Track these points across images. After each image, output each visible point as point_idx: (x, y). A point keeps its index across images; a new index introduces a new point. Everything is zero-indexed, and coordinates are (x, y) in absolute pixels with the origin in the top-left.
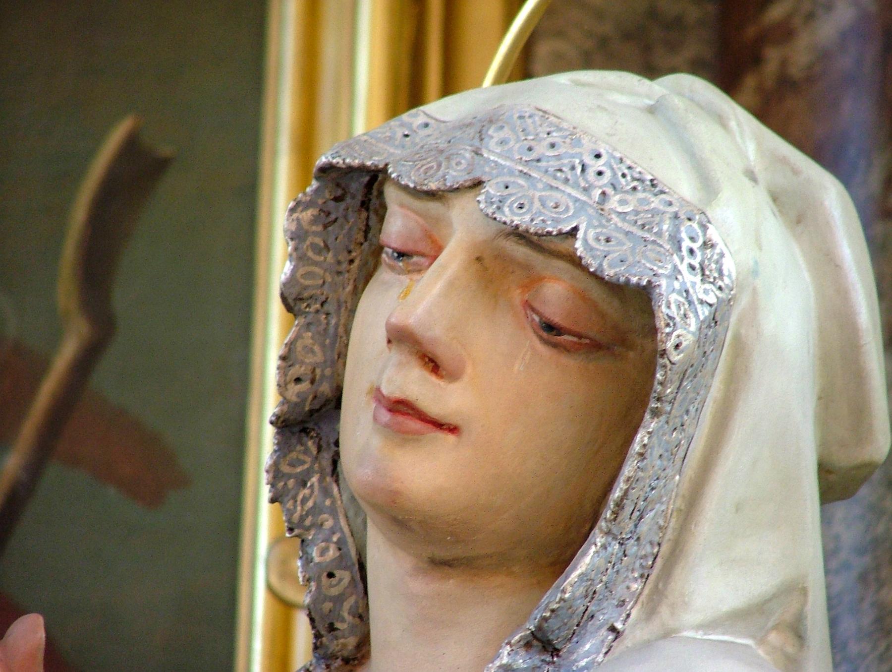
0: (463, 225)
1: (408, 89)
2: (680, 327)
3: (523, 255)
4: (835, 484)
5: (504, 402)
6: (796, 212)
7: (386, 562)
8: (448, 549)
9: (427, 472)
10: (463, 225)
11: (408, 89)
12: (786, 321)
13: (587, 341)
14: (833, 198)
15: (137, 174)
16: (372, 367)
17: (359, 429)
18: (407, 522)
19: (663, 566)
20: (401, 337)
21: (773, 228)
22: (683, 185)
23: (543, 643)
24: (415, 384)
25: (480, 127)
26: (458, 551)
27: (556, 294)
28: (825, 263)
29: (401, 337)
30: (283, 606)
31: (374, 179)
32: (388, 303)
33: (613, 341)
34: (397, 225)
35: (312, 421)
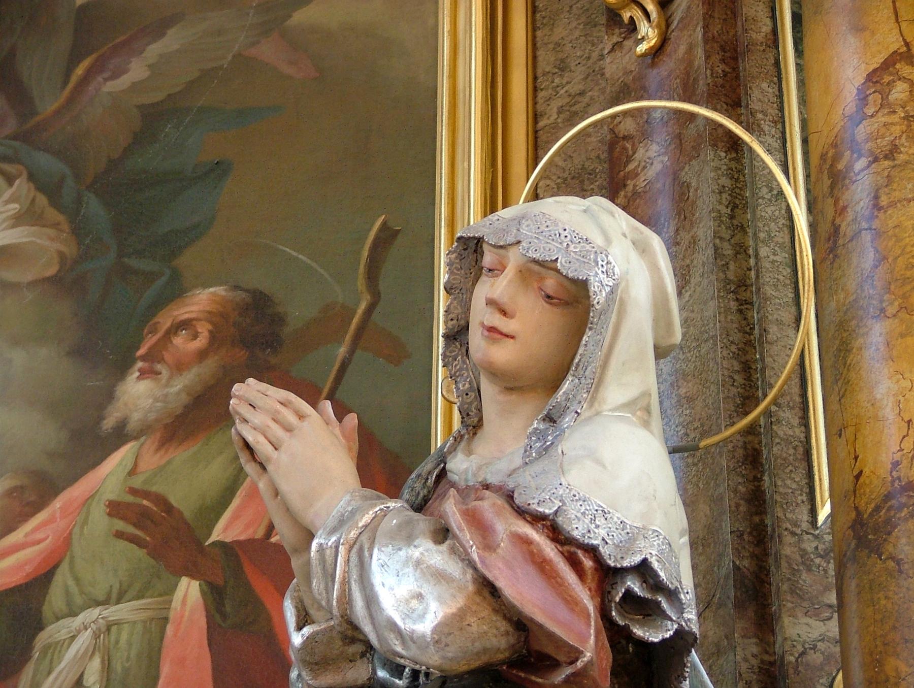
0: (514, 258)
1: (490, 207)
2: (599, 296)
3: (537, 270)
4: (660, 353)
5: (523, 330)
6: (642, 248)
7: (488, 389)
8: (512, 383)
9: (503, 354)
10: (514, 258)
11: (490, 207)
14: (656, 243)
15: (387, 237)
16: (480, 315)
17: (476, 338)
18: (496, 374)
19: (595, 387)
20: (491, 302)
21: (634, 255)
22: (599, 241)
23: (550, 419)
25: (519, 220)
27: (551, 284)
28: (654, 268)
29: (491, 302)
31: (479, 241)
32: (485, 289)
33: (574, 302)
34: (488, 259)
35: (458, 335)
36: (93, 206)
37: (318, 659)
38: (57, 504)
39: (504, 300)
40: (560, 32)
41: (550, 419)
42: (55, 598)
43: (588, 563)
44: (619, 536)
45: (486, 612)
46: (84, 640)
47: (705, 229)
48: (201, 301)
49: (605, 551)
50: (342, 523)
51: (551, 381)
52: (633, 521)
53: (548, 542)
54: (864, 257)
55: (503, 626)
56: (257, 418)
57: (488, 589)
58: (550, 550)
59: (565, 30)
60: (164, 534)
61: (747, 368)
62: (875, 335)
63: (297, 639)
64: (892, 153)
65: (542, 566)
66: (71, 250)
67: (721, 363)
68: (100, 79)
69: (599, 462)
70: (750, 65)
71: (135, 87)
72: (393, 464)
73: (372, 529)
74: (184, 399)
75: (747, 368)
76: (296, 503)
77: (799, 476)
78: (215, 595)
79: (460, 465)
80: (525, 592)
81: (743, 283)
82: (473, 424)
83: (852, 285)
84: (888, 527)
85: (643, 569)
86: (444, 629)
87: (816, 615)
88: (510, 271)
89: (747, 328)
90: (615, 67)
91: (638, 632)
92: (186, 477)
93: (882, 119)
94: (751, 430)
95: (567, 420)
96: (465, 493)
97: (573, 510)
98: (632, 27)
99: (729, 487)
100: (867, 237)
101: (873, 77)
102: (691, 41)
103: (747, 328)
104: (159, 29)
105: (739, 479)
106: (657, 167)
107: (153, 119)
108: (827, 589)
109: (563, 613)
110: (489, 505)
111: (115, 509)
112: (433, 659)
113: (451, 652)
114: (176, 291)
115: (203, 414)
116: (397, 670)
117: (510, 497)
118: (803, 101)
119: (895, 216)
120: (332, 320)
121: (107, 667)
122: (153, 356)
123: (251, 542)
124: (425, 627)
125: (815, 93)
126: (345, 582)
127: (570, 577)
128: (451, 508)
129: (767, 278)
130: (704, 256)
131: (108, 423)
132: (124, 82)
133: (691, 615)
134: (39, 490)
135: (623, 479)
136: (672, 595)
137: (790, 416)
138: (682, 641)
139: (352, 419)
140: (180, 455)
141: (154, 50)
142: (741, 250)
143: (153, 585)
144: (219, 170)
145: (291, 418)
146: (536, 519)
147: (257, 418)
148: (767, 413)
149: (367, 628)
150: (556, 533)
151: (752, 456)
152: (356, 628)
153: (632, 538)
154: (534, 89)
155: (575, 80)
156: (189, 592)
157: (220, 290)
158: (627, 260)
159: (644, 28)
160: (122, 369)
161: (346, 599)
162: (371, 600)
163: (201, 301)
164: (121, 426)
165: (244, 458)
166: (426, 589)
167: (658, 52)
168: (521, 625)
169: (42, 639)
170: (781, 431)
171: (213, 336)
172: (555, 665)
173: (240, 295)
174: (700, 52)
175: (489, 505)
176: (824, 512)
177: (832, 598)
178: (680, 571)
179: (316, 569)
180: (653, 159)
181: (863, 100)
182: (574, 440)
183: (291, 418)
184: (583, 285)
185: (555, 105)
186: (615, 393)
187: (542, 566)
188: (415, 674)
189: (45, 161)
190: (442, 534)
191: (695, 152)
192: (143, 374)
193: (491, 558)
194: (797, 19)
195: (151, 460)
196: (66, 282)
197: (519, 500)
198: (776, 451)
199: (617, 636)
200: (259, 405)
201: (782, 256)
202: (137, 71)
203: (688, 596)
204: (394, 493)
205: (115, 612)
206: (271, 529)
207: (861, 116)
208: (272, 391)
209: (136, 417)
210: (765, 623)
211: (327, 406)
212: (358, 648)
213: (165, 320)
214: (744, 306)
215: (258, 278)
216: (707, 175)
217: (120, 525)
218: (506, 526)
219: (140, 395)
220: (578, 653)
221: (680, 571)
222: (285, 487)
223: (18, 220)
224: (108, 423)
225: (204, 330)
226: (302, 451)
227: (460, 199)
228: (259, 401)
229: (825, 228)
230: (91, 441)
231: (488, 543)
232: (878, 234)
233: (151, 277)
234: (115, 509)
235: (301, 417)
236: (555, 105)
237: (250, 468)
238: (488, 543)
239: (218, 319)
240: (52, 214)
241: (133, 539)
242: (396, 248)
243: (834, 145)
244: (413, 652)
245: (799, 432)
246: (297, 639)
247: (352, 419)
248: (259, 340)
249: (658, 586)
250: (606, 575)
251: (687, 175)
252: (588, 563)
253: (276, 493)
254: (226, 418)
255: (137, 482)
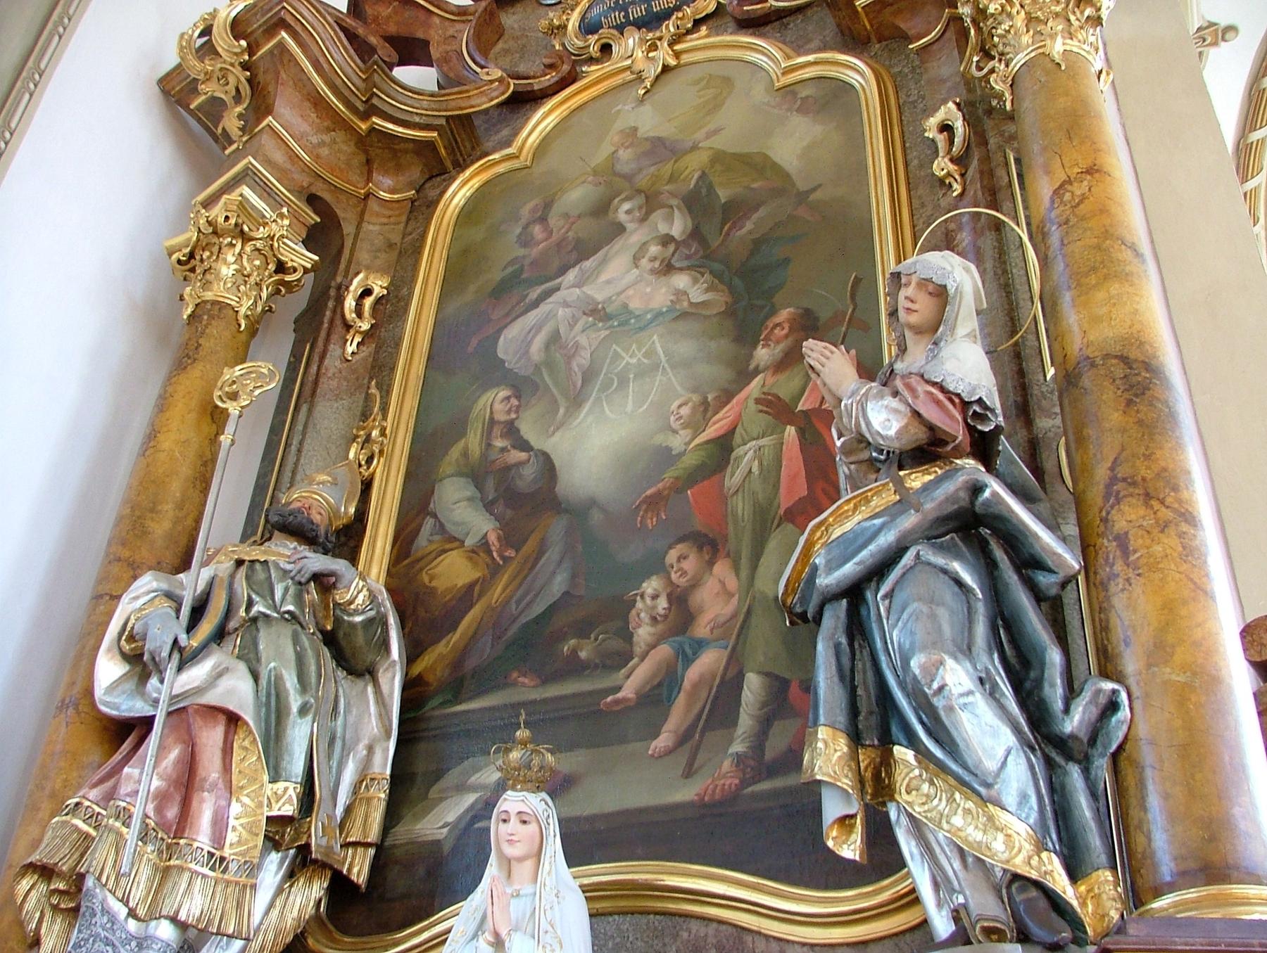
0: (914, 279)
1: (899, 262)
2: (951, 291)
3: (924, 283)
4: (978, 313)
5: (924, 307)
6: (967, 270)
7: (908, 334)
8: (918, 330)
9: (913, 319)
10: (914, 279)
11: (899, 262)
12: (968, 289)
13: (644, 507)
14: (973, 267)
15: (857, 281)
16: (902, 303)
17: (901, 313)
18: (911, 327)
19: (953, 329)
20: (906, 298)
21: (964, 273)
22: (949, 268)
23: (935, 343)
24: (910, 305)
25: (915, 263)
26: (532, 560)
27: (931, 288)
28: (973, 278)
29: (906, 298)
30: (890, 346)
31: (899, 273)
32: (903, 293)
33: (941, 294)
34: (903, 280)
35: (893, 314)
36: (737, 281)
37: (847, 451)
38: (734, 401)
39: (912, 297)
40: (920, 192)
41: (935, 343)
42: (737, 438)
43: (957, 401)
44: (968, 388)
45: (916, 424)
46: (751, 453)
47: (989, 265)
48: (784, 314)
49: (963, 395)
50: (853, 394)
51: (934, 329)
52: (974, 382)
53: (1116, 174)
54: (1059, 266)
55: (924, 429)
56: (814, 355)
57: (916, 414)
58: (941, 396)
59: (922, 191)
60: (779, 410)
61: (1012, 319)
62: (1067, 298)
63: (838, 443)
64: (1067, 222)
65: (938, 402)
66: (729, 300)
67: (1001, 318)
68: (491, 776)
69: (958, 359)
70: (1000, 196)
71: (750, 232)
72: (869, 369)
73: (866, 394)
74: (781, 355)
75: (1012, 319)
76: (833, 388)
77: (1038, 361)
78: (801, 432)
79: (899, 366)
80: (931, 414)
81: (1007, 285)
82: (903, 349)
83: (1055, 278)
84: (1079, 376)
85: (980, 401)
86: (899, 432)
87: (1050, 417)
88: (913, 284)
89: (1010, 303)
90: (944, 203)
91: (979, 427)
92: (785, 386)
93: (1062, 208)
94: (1016, 344)
95: (942, 344)
96: (903, 377)
97: (949, 380)
98: (950, 185)
99: (1010, 368)
100: (1060, 257)
101: (1056, 192)
102: (976, 188)
103: (1010, 303)
104: (756, 209)
105: (1014, 365)
106: (967, 241)
107: (758, 244)
108: (1054, 406)
109: (948, 421)
110: (914, 381)
111: (757, 401)
112: (896, 445)
113: (904, 441)
114: (773, 312)
115: (792, 358)
116: (881, 452)
117: (922, 376)
118: (1026, 208)
119: (1070, 248)
120: (837, 318)
121: (761, 464)
122: (767, 339)
123: (813, 410)
124: (892, 432)
125: (1032, 203)
126: (857, 418)
127: (950, 407)
128: (898, 383)
129: (1017, 281)
130: (990, 274)
131: (752, 367)
132: (744, 230)
133: (1001, 419)
134: (727, 396)
135: (968, 366)
136: (993, 411)
137: (1031, 337)
138: (998, 430)
139: (853, 352)
140: (782, 377)
141: (755, 216)
142: (1005, 272)
143: (777, 429)
144: (787, 261)
145: (828, 353)
146: (934, 384)
147: (814, 355)
148: (1022, 337)
149: (868, 436)
150: (942, 389)
151: (1017, 354)
152: (863, 436)
153: (973, 390)
154: (912, 215)
155: (929, 210)
156: (791, 431)
157: (792, 310)
158: (961, 275)
159: (955, 186)
160: (754, 346)
161: (858, 424)
162: (868, 424)
163: (784, 314)
164: (757, 366)
165: (810, 372)
166: (891, 417)
167: (962, 195)
168: (931, 428)
169: (734, 455)
170: (1028, 343)
171: (790, 328)
172: (947, 443)
173: (800, 311)
174: (980, 193)
175: (914, 381)
176: (1051, 372)
177: (1057, 410)
178: (995, 401)
179: (844, 413)
180: (965, 238)
181: (1053, 201)
182: (946, 351)
183: (828, 353)
184: (945, 286)
185: (921, 221)
186: (961, 331)
187: (938, 402)
188: (888, 452)
189: (717, 266)
190: (896, 394)
191: (982, 233)
192: (764, 346)
193: (917, 401)
194: (1020, 176)
195: (770, 380)
196: (730, 312)
197: (926, 377)
198: (1027, 352)
199: (971, 429)
200: (814, 349)
201: (1023, 272)
202: (749, 226)
203: (999, 411)
204: (873, 381)
205: (762, 442)
206: (823, 400)
207: (1052, 208)
208: (819, 343)
209: (762, 363)
210: (1029, 423)
211: (842, 347)
212: (863, 445)
213: (770, 324)
214: (1009, 294)
215: (806, 304)
216: (988, 242)
217: (761, 407)
218: (922, 388)
219: (763, 355)
220: (956, 438)
221: (995, 401)
222: (828, 381)
223: (707, 290)
224: (752, 367)
225: (786, 326)
226: (833, 365)
227: (886, 260)
228: (814, 348)
229: (1042, 255)
230: (745, 375)
231: (915, 397)
232: (1064, 256)
233: (763, 307)
234: (757, 401)
235: (832, 352)
236: (921, 221)
237: (813, 376)
238: (915, 397)
239: (792, 321)
240: (721, 287)
241: (766, 412)
242: (862, 286)
243: (1042, 222)
244: (888, 443)
245: (1036, 344)
246: (838, 443)
247: (853, 352)
248: (809, 326)
249: (986, 408)
250: (965, 405)
251: (979, 243)
252: (957, 401)
253: (825, 385)
254: (802, 357)
255: (765, 390)
